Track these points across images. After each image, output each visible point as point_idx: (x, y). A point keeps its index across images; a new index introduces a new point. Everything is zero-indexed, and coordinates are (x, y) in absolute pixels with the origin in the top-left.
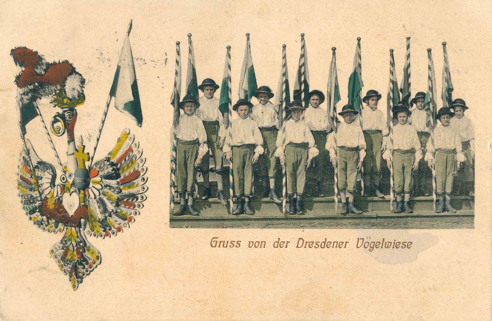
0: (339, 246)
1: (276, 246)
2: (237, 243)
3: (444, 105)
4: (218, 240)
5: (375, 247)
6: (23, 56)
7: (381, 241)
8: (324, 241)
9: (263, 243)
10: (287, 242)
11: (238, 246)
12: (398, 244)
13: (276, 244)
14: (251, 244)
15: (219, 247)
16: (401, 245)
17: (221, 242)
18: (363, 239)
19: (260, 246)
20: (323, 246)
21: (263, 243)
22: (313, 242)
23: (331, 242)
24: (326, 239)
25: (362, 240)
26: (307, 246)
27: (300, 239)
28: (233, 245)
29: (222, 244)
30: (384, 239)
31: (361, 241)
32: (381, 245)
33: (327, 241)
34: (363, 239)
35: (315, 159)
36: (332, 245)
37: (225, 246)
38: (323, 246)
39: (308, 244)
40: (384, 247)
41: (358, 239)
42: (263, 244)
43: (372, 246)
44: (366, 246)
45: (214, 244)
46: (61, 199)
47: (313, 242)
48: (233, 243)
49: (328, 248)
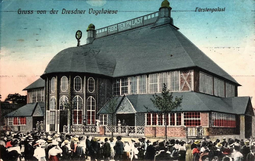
0: (53, 12)
1: (51, 13)
2: (32, 12)
5: (98, 13)
6: (55, 149)
8: (52, 10)
11: (32, 13)
12: (82, 11)
13: (51, 12)
15: (22, 13)
17: (23, 11)
18: (92, 9)
20: (75, 13)
22: (70, 11)
23: (55, 11)
24: (77, 9)
25: (92, 10)
26: (23, 13)
28: (29, 12)
29: (24, 12)
30: (103, 9)
31: (91, 10)
32: (101, 12)
33: (54, 10)
34: (92, 9)
35: (9, 103)
38: (75, 13)
39: (68, 12)
40: (206, 11)
41: (90, 9)
42: (44, 12)
43: (97, 12)
44: (94, 12)
45: (20, 12)
48: (73, 11)
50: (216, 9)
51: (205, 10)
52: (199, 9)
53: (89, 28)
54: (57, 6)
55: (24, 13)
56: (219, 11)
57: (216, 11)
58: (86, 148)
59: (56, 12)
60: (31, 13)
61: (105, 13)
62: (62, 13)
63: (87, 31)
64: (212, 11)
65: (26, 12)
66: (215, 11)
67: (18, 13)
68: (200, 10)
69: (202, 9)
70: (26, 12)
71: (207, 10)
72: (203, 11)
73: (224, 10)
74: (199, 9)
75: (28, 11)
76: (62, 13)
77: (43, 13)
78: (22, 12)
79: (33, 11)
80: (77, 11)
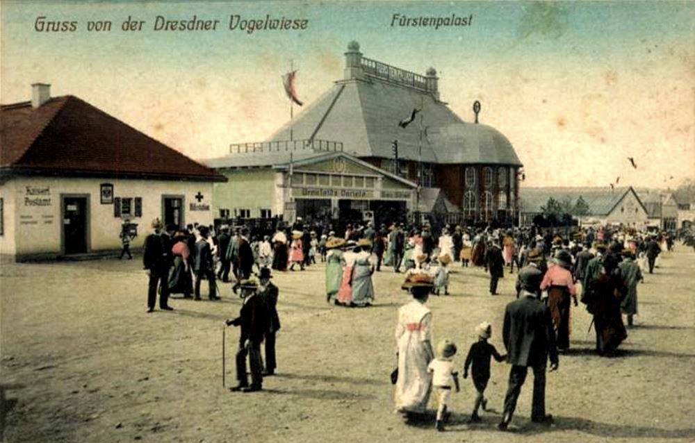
3: (411, 301)
4: (46, 21)
7: (264, 19)
8: (193, 19)
9: (108, 24)
10: (141, 23)
11: (73, 28)
14: (91, 25)
16: (292, 24)
17: (49, 23)
18: (239, 17)
19: (279, 26)
20: (190, 27)
21: (108, 24)
27: (158, 17)
28: (66, 26)
31: (235, 20)
32: (429, 22)
34: (239, 17)
36: (429, 22)
37: (55, 28)
38: (190, 27)
39: (51, 26)
40: (169, 27)
41: (232, 17)
42: (107, 25)
43: (251, 26)
45: (40, 26)
46: (575, 278)
47: (177, 22)
49: (302, 28)
50: (449, 19)
51: (418, 21)
52: (401, 20)
53: (349, 48)
54: (221, 13)
55: (53, 29)
56: (456, 24)
57: (448, 24)
58: (277, 333)
59: (212, 25)
60: (71, 30)
61: (274, 27)
62: (155, 29)
63: (346, 54)
64: (438, 25)
65: (56, 25)
66: (246, 21)
67: (36, 27)
68: (404, 22)
69: (409, 20)
70: (56, 25)
71: (424, 22)
72: (413, 25)
73: (468, 20)
74: (401, 20)
75: (414, 20)
76: (155, 29)
77: (104, 30)
78: (46, 26)
79: (76, 22)
80: (196, 25)
